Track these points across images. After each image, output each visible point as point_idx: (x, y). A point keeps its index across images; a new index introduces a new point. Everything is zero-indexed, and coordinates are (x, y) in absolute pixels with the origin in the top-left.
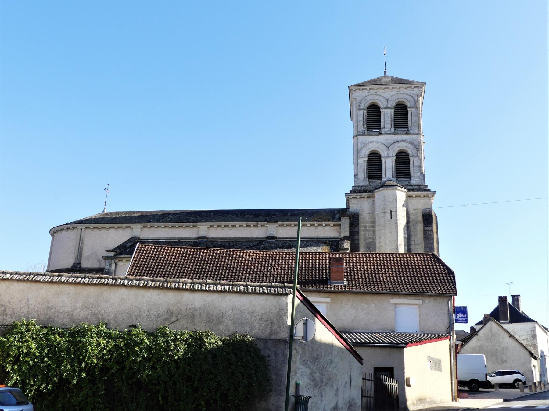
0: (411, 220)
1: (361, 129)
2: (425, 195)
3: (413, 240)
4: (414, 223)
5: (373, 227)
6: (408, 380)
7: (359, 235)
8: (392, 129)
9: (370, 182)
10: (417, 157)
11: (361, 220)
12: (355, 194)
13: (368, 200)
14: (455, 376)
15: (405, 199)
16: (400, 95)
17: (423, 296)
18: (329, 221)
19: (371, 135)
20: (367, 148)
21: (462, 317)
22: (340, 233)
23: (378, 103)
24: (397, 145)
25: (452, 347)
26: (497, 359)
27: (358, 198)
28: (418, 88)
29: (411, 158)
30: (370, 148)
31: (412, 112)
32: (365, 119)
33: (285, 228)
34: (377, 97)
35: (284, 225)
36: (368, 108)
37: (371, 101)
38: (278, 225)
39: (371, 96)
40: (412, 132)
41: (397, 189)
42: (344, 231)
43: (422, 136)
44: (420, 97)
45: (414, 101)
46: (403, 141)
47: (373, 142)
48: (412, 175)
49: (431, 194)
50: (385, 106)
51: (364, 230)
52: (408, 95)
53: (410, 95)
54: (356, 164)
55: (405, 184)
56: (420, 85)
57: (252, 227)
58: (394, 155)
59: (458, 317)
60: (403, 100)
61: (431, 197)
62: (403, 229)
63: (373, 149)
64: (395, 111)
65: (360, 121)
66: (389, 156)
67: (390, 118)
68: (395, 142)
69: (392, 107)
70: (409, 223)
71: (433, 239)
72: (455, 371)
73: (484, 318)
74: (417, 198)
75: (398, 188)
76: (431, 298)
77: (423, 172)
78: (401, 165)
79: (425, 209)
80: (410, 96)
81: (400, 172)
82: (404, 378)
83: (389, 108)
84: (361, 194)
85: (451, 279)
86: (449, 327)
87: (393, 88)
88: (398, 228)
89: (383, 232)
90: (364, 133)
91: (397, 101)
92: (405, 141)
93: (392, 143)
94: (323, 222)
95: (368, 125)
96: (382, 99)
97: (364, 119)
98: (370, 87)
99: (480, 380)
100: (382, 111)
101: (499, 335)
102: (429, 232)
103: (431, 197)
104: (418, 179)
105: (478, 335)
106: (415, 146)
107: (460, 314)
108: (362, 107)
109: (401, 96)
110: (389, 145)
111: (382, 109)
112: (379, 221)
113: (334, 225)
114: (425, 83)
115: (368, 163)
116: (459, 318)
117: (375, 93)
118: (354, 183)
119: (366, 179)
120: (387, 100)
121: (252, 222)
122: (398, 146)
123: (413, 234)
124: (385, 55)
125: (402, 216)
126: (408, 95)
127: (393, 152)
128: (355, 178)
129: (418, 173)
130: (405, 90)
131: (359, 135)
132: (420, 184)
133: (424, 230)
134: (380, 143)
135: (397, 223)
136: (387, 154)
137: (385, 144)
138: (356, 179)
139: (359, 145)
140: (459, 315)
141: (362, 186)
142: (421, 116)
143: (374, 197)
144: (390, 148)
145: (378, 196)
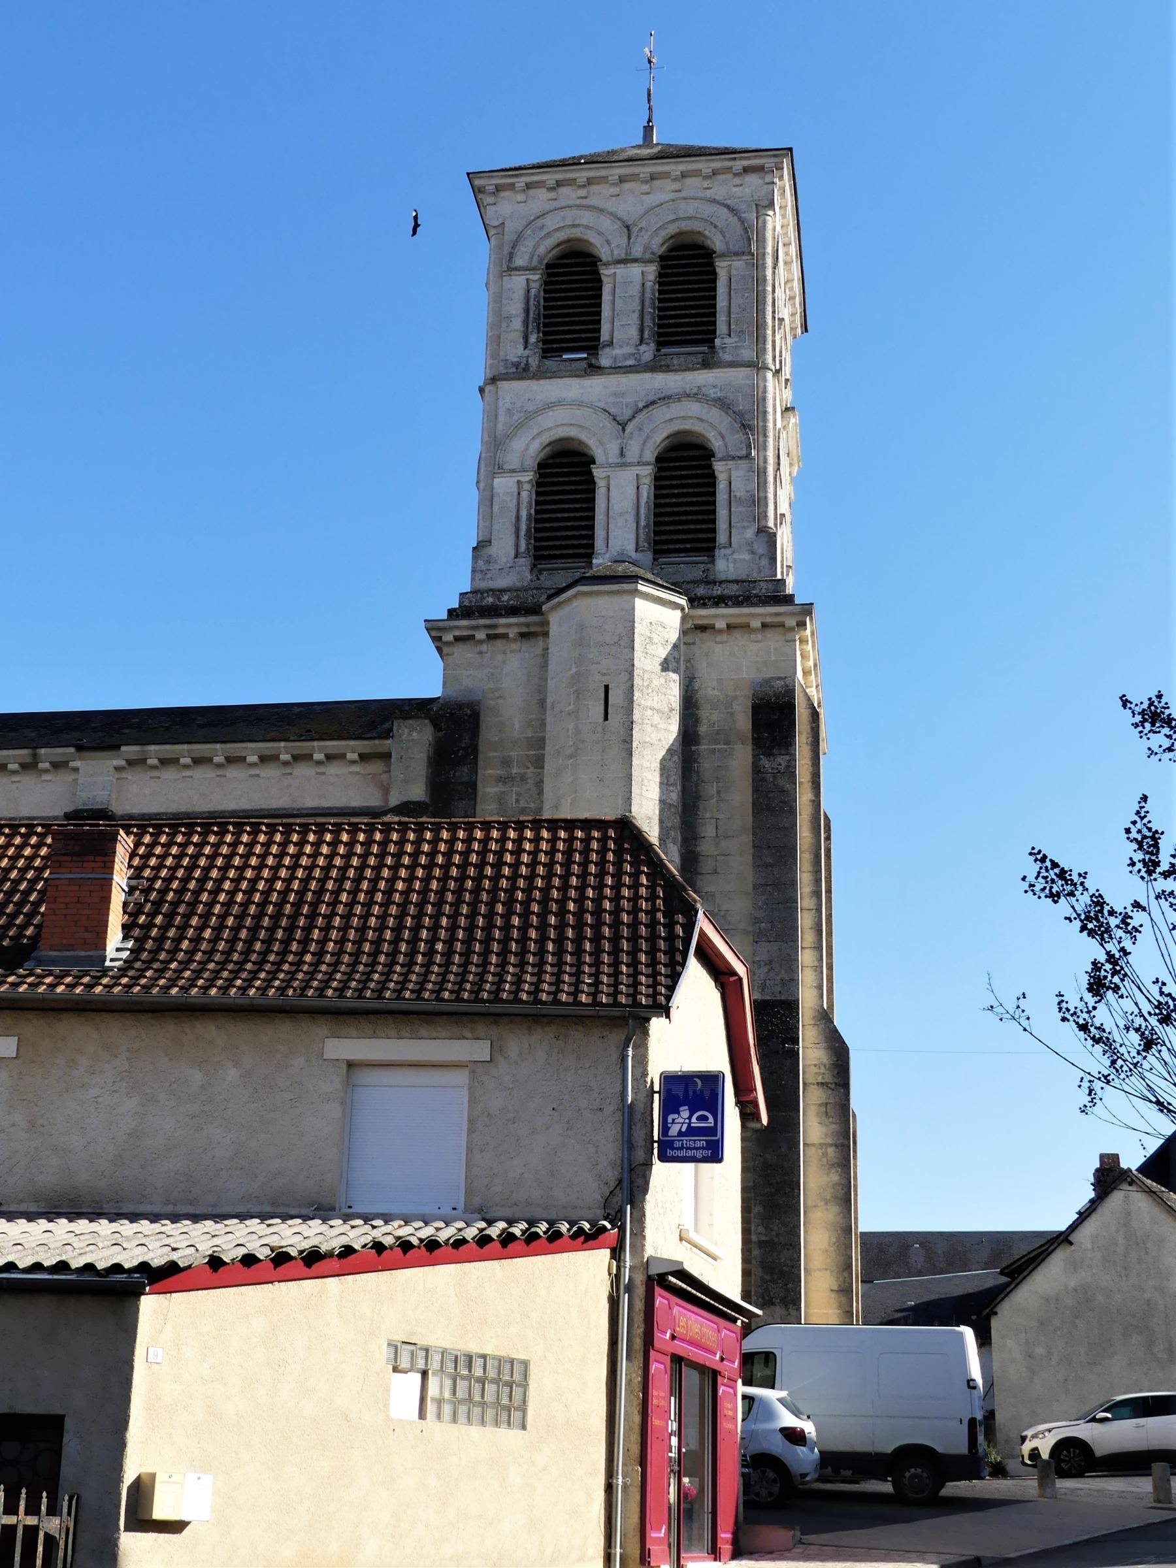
0: (703, 729)
1: (515, 350)
2: (768, 620)
3: (708, 815)
4: (716, 742)
5: (539, 763)
6: (142, 1491)
7: (475, 799)
8: (643, 348)
9: (541, 571)
10: (744, 464)
11: (488, 734)
12: (465, 623)
13: (525, 646)
14: (636, 1450)
15: (674, 635)
16: (683, 205)
17: (496, 1023)
18: (339, 738)
19: (553, 375)
20: (536, 431)
21: (691, 1131)
22: (386, 791)
23: (592, 240)
24: (662, 413)
25: (629, 1288)
26: (1150, 1344)
27: (482, 642)
28: (762, 174)
29: (719, 467)
30: (550, 429)
31: (734, 272)
32: (532, 309)
33: (155, 773)
34: (586, 218)
35: (150, 761)
36: (548, 266)
37: (561, 236)
38: (122, 763)
39: (560, 213)
40: (727, 357)
41: (637, 590)
42: (405, 781)
43: (769, 375)
44: (771, 213)
45: (739, 229)
46: (688, 396)
47: (559, 403)
48: (722, 538)
49: (794, 614)
50: (619, 253)
51: (503, 780)
52: (718, 203)
53: (728, 207)
54: (488, 499)
55: (689, 577)
56: (768, 162)
57: (14, 772)
58: (650, 455)
59: (674, 1130)
60: (697, 226)
61: (792, 629)
62: (656, 765)
63: (562, 433)
64: (660, 275)
65: (509, 318)
66: (628, 459)
67: (637, 301)
68: (653, 403)
69: (647, 256)
70: (697, 744)
71: (792, 812)
72: (637, 1419)
73: (1097, 1170)
74: (737, 634)
75: (642, 587)
76: (538, 1033)
77: (771, 524)
78: (680, 500)
79: (768, 681)
80: (726, 210)
81: (672, 528)
82: (119, 1480)
83: (635, 260)
84: (494, 621)
85: (671, 937)
86: (620, 1181)
87: (653, 177)
88: (635, 761)
89: (570, 780)
90: (526, 368)
91: (673, 229)
92: (695, 395)
93: (641, 405)
94: (316, 743)
95: (545, 333)
96: (607, 224)
97: (527, 311)
98: (559, 176)
99: (940, 1449)
100: (605, 272)
101: (1161, 1242)
102: (775, 777)
103: (792, 629)
104: (747, 556)
105: (1071, 1244)
106: (739, 415)
107: (685, 1114)
108: (519, 262)
109: (690, 209)
110: (627, 413)
111: (607, 264)
112: (559, 732)
113: (364, 757)
114: (790, 149)
115: (538, 494)
116: (680, 1134)
117: (579, 202)
118: (473, 579)
119: (525, 563)
120: (628, 227)
121: (11, 752)
122: (668, 417)
123: (711, 789)
124: (650, 62)
125: (658, 711)
126: (718, 203)
127: (644, 443)
128: (475, 558)
129: (747, 527)
130: (706, 184)
131: (505, 377)
132: (755, 576)
133: (757, 770)
134: (591, 406)
135: (628, 741)
136: (617, 451)
137: (613, 411)
138: (480, 563)
139: (502, 418)
140: (682, 1119)
141: (502, 591)
142: (769, 289)
143: (546, 634)
144: (629, 429)
145: (560, 625)
